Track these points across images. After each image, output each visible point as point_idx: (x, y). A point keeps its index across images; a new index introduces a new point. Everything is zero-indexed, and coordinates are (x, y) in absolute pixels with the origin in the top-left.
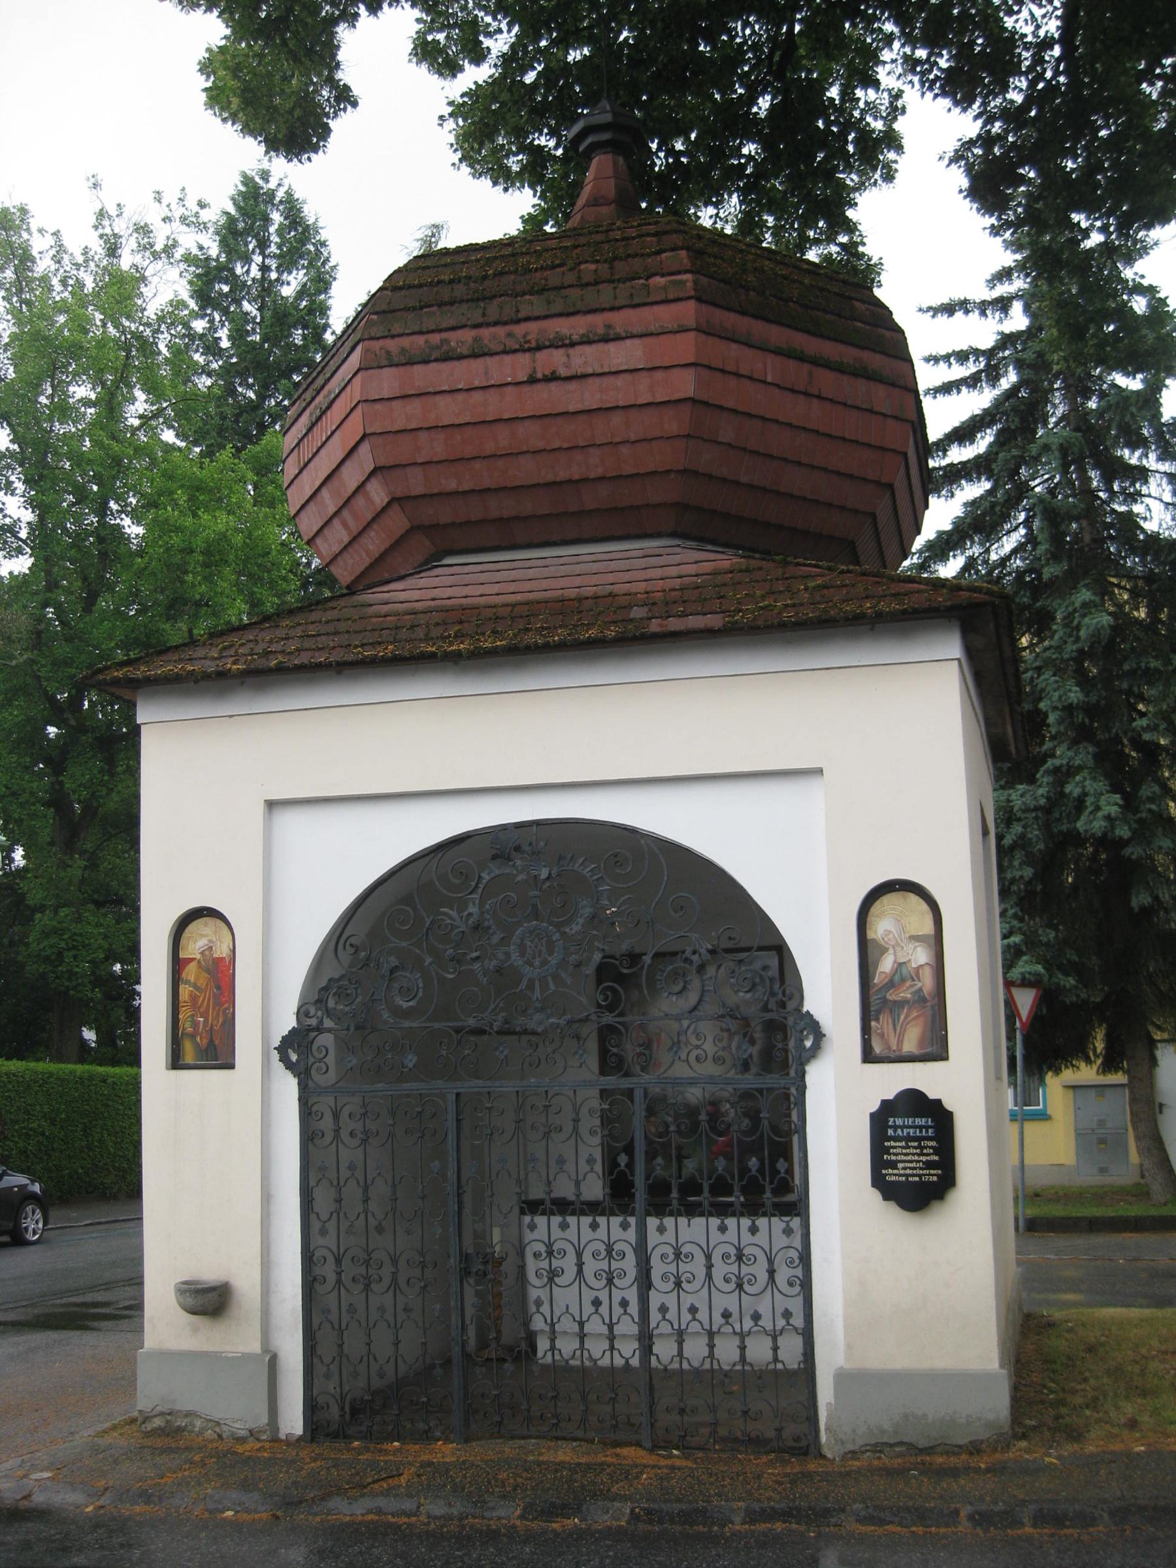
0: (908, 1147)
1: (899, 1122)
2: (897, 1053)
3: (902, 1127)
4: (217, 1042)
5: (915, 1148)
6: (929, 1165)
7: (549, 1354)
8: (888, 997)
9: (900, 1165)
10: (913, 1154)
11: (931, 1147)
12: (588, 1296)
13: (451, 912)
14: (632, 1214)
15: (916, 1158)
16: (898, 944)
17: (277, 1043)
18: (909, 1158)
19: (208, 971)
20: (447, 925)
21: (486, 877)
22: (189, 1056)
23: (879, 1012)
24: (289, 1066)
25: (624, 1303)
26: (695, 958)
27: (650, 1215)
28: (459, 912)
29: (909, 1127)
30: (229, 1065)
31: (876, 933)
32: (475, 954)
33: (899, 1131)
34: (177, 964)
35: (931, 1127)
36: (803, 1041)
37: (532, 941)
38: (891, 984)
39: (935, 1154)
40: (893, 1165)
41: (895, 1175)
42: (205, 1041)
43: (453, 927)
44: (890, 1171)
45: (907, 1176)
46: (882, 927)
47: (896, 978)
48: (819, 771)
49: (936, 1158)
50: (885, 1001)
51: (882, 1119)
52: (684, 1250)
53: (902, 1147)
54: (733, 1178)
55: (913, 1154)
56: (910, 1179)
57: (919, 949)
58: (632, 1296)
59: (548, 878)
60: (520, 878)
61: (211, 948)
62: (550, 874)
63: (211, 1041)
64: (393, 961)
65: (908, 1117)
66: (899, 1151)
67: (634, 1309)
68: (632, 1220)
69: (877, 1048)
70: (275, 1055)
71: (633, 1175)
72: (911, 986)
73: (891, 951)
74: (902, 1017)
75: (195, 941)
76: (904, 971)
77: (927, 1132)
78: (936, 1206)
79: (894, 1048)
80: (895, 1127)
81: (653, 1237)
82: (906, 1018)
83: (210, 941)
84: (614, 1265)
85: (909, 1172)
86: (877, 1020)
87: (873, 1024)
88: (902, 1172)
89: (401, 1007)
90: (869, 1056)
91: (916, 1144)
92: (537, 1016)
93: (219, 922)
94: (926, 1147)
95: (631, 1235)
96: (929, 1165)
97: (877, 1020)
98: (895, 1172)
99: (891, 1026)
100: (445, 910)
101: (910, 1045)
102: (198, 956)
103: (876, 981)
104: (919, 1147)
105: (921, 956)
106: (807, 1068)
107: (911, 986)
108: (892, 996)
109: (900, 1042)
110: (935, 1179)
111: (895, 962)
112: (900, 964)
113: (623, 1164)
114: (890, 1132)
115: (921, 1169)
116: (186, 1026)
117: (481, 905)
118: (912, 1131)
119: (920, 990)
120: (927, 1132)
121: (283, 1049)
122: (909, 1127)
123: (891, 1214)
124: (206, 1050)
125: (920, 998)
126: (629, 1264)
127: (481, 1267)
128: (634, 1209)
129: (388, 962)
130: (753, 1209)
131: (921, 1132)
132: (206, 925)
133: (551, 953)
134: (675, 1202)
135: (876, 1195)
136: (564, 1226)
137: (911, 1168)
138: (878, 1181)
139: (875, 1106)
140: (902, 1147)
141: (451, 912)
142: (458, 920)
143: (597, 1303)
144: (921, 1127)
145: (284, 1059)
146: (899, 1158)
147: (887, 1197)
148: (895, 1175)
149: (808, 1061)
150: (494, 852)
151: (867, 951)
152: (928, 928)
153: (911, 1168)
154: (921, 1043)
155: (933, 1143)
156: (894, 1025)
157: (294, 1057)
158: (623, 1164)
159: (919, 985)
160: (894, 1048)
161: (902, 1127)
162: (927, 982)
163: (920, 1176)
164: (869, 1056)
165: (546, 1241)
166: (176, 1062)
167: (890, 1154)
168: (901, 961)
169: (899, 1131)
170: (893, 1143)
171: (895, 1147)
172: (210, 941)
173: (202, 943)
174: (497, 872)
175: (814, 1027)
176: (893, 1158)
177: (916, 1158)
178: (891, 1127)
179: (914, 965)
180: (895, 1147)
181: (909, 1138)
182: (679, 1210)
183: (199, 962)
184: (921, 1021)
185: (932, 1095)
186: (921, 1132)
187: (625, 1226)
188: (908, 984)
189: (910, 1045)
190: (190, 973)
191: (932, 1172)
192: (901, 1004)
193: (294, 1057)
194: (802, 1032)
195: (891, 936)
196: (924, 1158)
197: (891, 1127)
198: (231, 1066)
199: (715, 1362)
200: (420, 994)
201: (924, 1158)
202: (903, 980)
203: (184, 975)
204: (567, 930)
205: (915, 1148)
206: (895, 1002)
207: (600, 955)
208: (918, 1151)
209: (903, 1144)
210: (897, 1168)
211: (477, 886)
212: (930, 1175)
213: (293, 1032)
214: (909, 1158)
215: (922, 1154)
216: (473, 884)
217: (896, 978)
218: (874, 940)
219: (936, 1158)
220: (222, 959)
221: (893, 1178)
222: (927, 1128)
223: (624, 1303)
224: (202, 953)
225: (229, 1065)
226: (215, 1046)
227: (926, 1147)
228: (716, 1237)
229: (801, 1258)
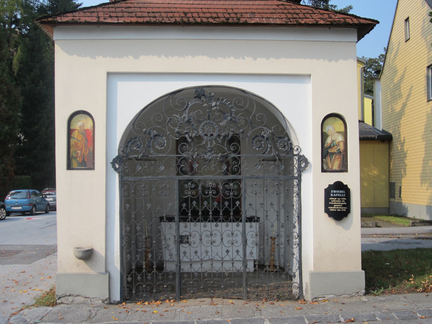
0: (337, 200)
1: (335, 192)
2: (331, 170)
3: (336, 193)
4: (86, 160)
5: (339, 200)
6: (344, 206)
7: (200, 269)
8: (329, 151)
9: (335, 206)
10: (339, 202)
11: (344, 200)
12: (225, 249)
13: (177, 116)
14: (241, 221)
15: (340, 203)
16: (333, 134)
17: (111, 161)
18: (338, 203)
19: (82, 134)
20: (176, 120)
21: (190, 105)
22: (75, 164)
23: (326, 156)
24: (116, 169)
25: (237, 252)
26: (265, 136)
27: (181, 222)
28: (180, 116)
29: (338, 193)
30: (92, 168)
31: (326, 130)
32: (186, 131)
33: (335, 195)
34: (70, 132)
35: (344, 193)
36: (300, 164)
37: (207, 127)
38: (330, 147)
39: (345, 202)
40: (332, 205)
41: (333, 209)
42: (81, 160)
43: (178, 121)
44: (331, 208)
45: (337, 209)
46: (329, 129)
47: (332, 145)
48: (310, 76)
49: (345, 203)
50: (328, 152)
51: (328, 191)
52: (235, 233)
53: (335, 200)
54: (209, 209)
55: (339, 202)
56: (338, 210)
57: (339, 136)
58: (241, 249)
59: (215, 106)
60: (205, 105)
61: (83, 126)
62: (216, 104)
63: (84, 160)
64: (155, 132)
65: (334, 190)
66: (334, 201)
67: (241, 253)
68: (241, 224)
69: (325, 168)
70: (111, 165)
71: (241, 208)
72: (336, 148)
73: (330, 136)
74: (333, 158)
75: (77, 123)
76: (334, 143)
77: (343, 195)
78: (345, 219)
79: (331, 168)
80: (333, 193)
81: (248, 229)
82: (335, 158)
83: (83, 123)
84: (234, 238)
85: (337, 208)
86: (325, 158)
87: (324, 160)
88: (335, 208)
89: (158, 149)
90: (323, 171)
91: (340, 199)
92: (209, 154)
93: (87, 116)
94: (343, 200)
95: (240, 228)
96: (344, 206)
97: (325, 158)
98: (333, 208)
99: (329, 160)
100: (173, 115)
101: (335, 167)
102: (78, 128)
103: (325, 146)
104: (341, 200)
105: (340, 138)
106: (302, 173)
107: (336, 148)
108: (330, 151)
109: (332, 166)
110: (345, 210)
111: (332, 140)
112: (333, 141)
113: (237, 205)
114: (332, 195)
115: (341, 207)
116: (73, 154)
117: (189, 114)
118: (339, 195)
119: (339, 149)
120: (343, 195)
121: (113, 163)
122: (338, 193)
123: (331, 221)
124: (82, 163)
125: (340, 152)
126: (239, 238)
127: (187, 240)
128: (241, 220)
129: (153, 133)
130: (227, 219)
131: (341, 195)
132: (81, 117)
133: (214, 132)
134: (190, 217)
135: (326, 215)
136: (205, 226)
137: (338, 207)
138: (327, 211)
139: (326, 187)
140: (335, 200)
141: (177, 116)
142: (180, 118)
143: (228, 251)
144: (341, 194)
145: (114, 167)
146: (334, 203)
147: (330, 216)
148: (333, 209)
149: (302, 171)
150: (196, 95)
151: (324, 136)
152: (342, 129)
153: (338, 207)
154: (339, 166)
155: (345, 199)
156: (331, 160)
157: (117, 166)
158: (237, 205)
159: (339, 148)
160: (331, 168)
161: (336, 193)
162: (342, 147)
163: (341, 209)
164: (323, 171)
165: (210, 231)
166: (69, 167)
167: (331, 202)
168: (334, 139)
169: (335, 195)
170: (332, 199)
171: (333, 200)
172: (83, 123)
173: (80, 124)
174: (195, 103)
175: (303, 159)
176: (332, 203)
177: (340, 203)
178: (332, 193)
179: (337, 141)
180: (333, 200)
181: (337, 197)
182: (202, 220)
183: (78, 130)
184: (339, 159)
185: (345, 184)
186: (341, 195)
187: (238, 226)
188: (336, 147)
189: (335, 167)
190: (75, 134)
191: (344, 208)
192: (333, 153)
193: (117, 166)
194: (300, 162)
195: (330, 131)
196: (342, 204)
197: (332, 193)
198: (93, 169)
199: (203, 269)
200: (165, 145)
201: (342, 204)
202: (334, 146)
203: (72, 135)
204: (220, 124)
205: (339, 200)
206: (331, 153)
207: (232, 133)
208: (340, 201)
209: (336, 199)
210: (333, 206)
211: (187, 107)
212: (344, 209)
213: (117, 157)
214: (338, 203)
215: (341, 202)
216: (185, 106)
217: (332, 145)
218: (325, 132)
219: (345, 203)
220: (87, 130)
221: (332, 210)
222: (343, 194)
223: (237, 252)
224: (80, 127)
225: (92, 168)
226: (85, 162)
227: (343, 200)
228: (203, 229)
229: (298, 236)
